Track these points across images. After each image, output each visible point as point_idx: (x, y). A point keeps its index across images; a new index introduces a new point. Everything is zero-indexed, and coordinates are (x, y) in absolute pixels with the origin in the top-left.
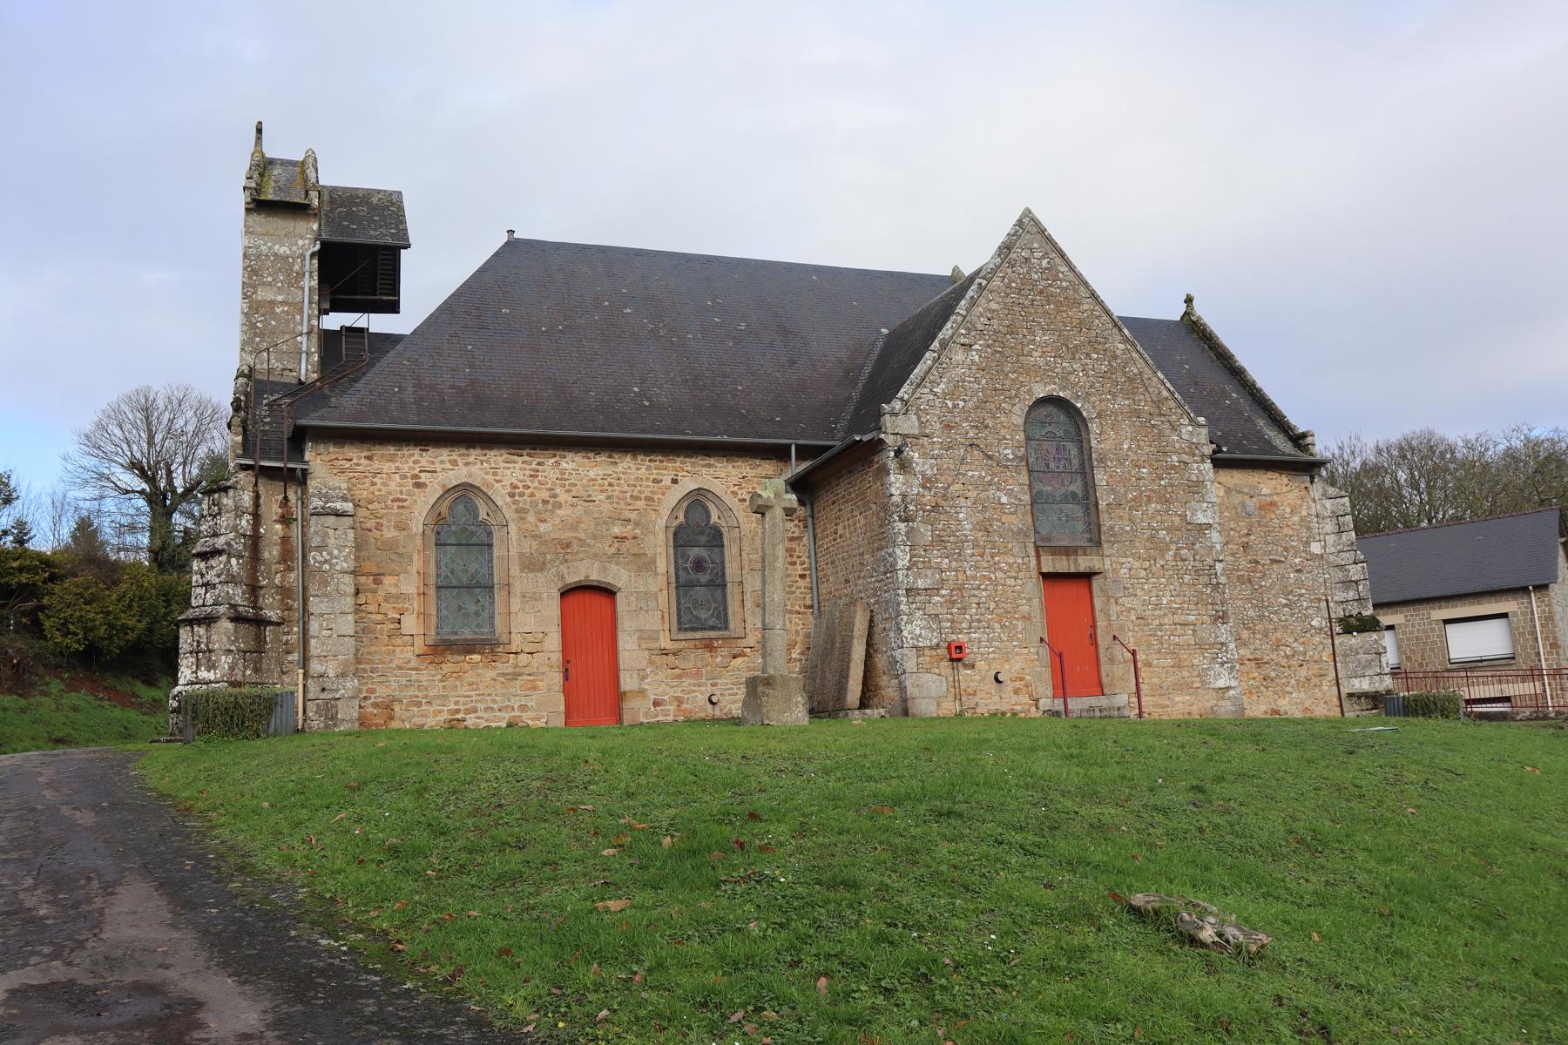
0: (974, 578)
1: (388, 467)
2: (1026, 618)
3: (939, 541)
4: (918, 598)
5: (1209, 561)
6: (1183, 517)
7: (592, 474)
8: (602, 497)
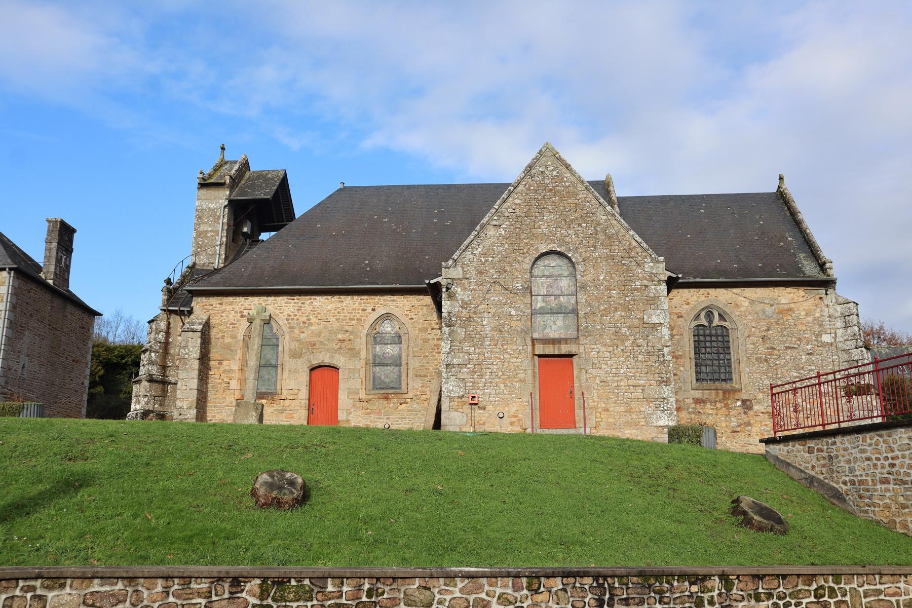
0: (490, 358)
1: (229, 308)
2: (522, 381)
3: (469, 338)
4: (453, 370)
5: (659, 346)
6: (642, 320)
7: (329, 308)
8: (334, 319)
